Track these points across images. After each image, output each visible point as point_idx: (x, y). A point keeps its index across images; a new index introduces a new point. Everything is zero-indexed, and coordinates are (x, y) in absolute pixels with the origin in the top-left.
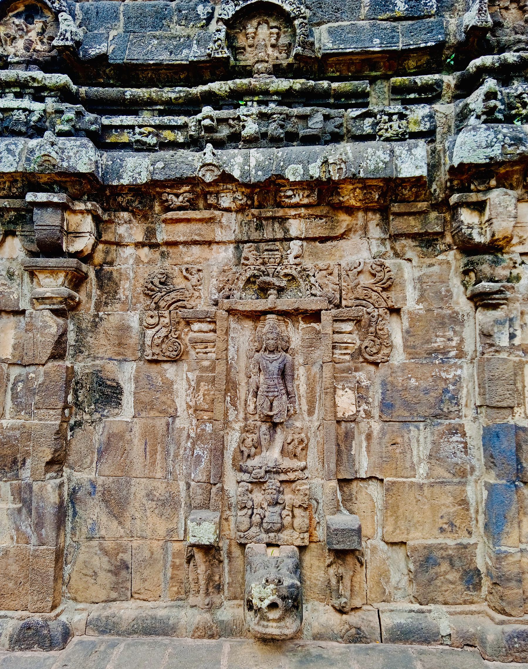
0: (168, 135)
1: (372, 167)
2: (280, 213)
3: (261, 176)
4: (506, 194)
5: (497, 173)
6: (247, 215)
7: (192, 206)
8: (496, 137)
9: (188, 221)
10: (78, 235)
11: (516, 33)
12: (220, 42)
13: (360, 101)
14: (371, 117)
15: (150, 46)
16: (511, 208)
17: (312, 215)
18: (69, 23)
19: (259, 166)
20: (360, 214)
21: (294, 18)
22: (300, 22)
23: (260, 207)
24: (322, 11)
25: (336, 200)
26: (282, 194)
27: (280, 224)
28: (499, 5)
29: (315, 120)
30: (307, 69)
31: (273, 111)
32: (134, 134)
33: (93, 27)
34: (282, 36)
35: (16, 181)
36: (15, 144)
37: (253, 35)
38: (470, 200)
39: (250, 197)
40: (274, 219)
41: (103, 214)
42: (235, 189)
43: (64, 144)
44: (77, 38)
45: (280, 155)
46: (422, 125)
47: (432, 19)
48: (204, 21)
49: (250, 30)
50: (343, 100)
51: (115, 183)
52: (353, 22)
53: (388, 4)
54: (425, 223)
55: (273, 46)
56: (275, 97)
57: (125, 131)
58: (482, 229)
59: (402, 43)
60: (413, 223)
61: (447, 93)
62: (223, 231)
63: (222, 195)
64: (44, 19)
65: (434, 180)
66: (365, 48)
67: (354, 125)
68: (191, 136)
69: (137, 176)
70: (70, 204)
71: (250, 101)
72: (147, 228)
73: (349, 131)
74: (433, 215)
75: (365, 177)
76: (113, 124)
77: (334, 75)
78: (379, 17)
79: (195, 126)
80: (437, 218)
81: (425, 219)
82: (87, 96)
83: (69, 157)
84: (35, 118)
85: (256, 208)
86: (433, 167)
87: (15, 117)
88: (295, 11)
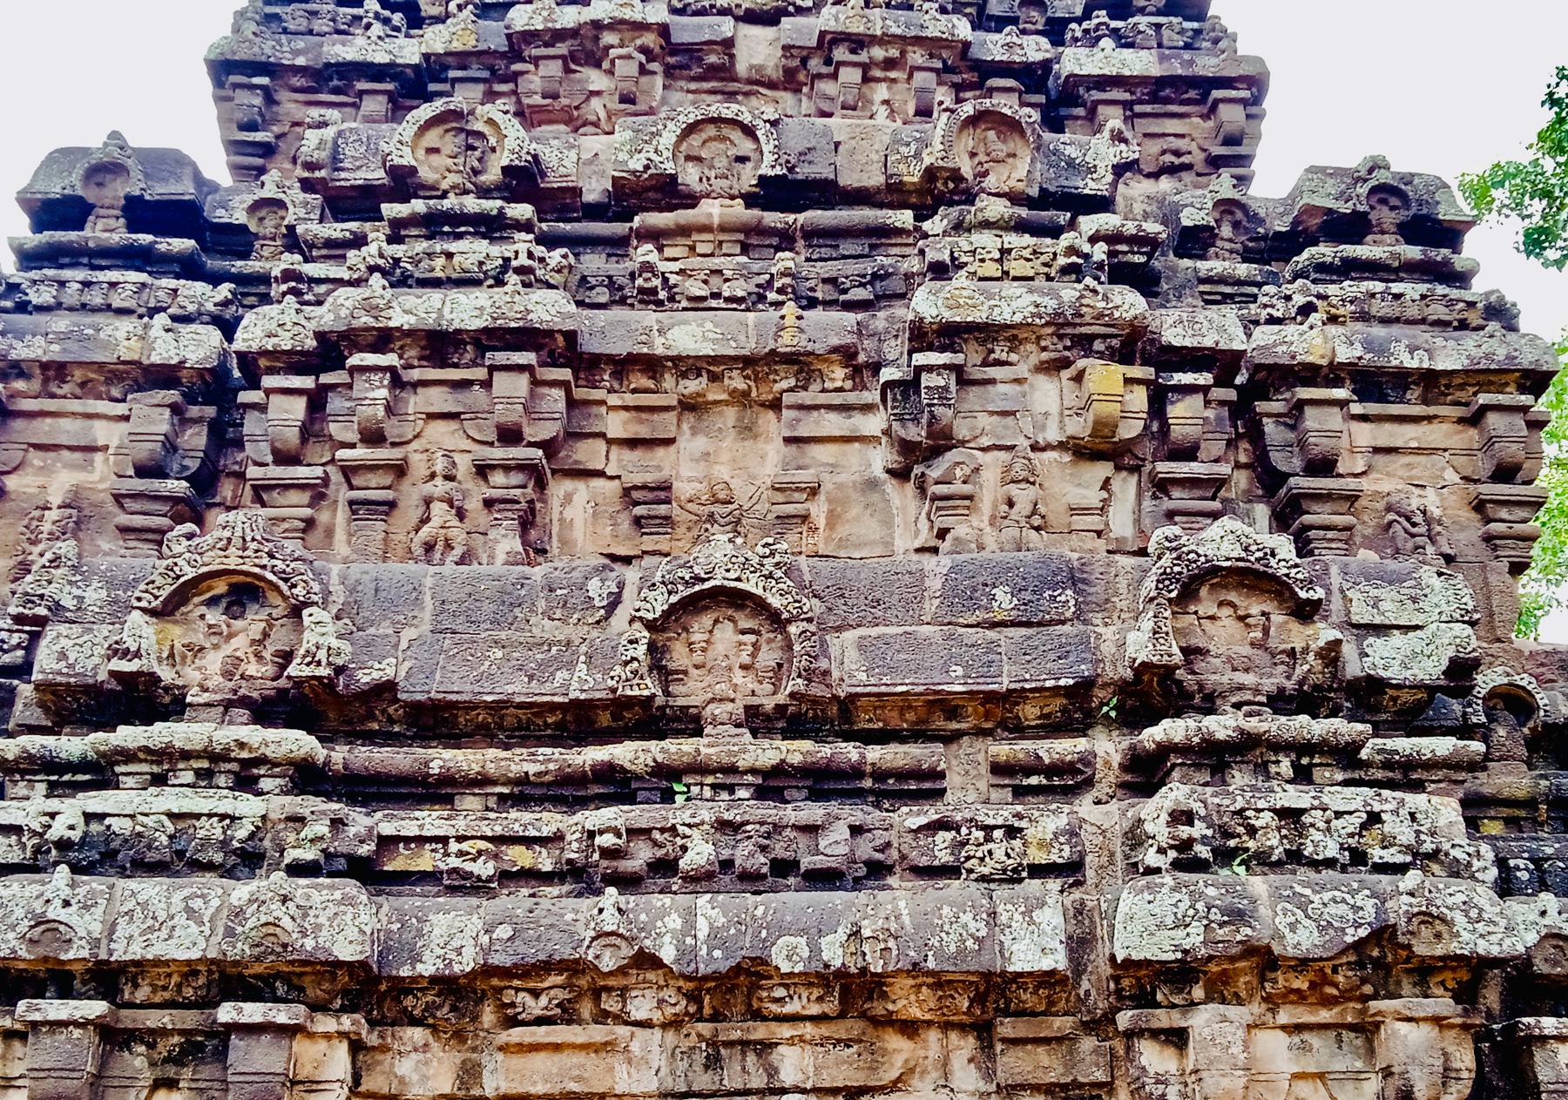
0: (520, 857)
1: (953, 948)
2: (760, 1031)
3: (719, 961)
4: (1224, 1019)
5: (1205, 973)
6: (687, 1035)
7: (568, 1015)
9: (557, 1047)
10: (315, 1087)
11: (1235, 669)
12: (635, 664)
13: (927, 785)
15: (487, 663)
16: (1236, 1049)
17: (828, 1038)
18: (324, 630)
20: (933, 1035)
21: (789, 621)
23: (716, 1017)
25: (878, 1008)
26: (765, 994)
27: (759, 1055)
28: (1196, 613)
29: (833, 837)
30: (815, 715)
31: (747, 817)
33: (366, 619)
34: (764, 648)
35: (196, 973)
36: (203, 896)
38: (1155, 1024)
39: (693, 997)
40: (744, 1044)
41: (370, 1032)
42: (662, 983)
43: (308, 897)
44: (340, 662)
45: (760, 912)
47: (1067, 628)
48: (602, 612)
49: (698, 638)
50: (891, 781)
51: (405, 972)
52: (908, 629)
54: (1071, 1063)
55: (744, 667)
56: (749, 778)
57: (427, 846)
58: (1186, 1085)
59: (1009, 676)
60: (1045, 1061)
61: (1107, 778)
62: (632, 1070)
63: (634, 993)
64: (268, 610)
68: (570, 862)
69: (453, 956)
70: (308, 1024)
72: (464, 1062)
73: (903, 857)
74: (1088, 1043)
76: (403, 833)
77: (871, 726)
79: (579, 840)
80: (1095, 1051)
81: (1070, 1053)
82: (345, 768)
83: (318, 927)
84: (242, 833)
85: (706, 1021)
86: (1079, 945)
87: (201, 833)
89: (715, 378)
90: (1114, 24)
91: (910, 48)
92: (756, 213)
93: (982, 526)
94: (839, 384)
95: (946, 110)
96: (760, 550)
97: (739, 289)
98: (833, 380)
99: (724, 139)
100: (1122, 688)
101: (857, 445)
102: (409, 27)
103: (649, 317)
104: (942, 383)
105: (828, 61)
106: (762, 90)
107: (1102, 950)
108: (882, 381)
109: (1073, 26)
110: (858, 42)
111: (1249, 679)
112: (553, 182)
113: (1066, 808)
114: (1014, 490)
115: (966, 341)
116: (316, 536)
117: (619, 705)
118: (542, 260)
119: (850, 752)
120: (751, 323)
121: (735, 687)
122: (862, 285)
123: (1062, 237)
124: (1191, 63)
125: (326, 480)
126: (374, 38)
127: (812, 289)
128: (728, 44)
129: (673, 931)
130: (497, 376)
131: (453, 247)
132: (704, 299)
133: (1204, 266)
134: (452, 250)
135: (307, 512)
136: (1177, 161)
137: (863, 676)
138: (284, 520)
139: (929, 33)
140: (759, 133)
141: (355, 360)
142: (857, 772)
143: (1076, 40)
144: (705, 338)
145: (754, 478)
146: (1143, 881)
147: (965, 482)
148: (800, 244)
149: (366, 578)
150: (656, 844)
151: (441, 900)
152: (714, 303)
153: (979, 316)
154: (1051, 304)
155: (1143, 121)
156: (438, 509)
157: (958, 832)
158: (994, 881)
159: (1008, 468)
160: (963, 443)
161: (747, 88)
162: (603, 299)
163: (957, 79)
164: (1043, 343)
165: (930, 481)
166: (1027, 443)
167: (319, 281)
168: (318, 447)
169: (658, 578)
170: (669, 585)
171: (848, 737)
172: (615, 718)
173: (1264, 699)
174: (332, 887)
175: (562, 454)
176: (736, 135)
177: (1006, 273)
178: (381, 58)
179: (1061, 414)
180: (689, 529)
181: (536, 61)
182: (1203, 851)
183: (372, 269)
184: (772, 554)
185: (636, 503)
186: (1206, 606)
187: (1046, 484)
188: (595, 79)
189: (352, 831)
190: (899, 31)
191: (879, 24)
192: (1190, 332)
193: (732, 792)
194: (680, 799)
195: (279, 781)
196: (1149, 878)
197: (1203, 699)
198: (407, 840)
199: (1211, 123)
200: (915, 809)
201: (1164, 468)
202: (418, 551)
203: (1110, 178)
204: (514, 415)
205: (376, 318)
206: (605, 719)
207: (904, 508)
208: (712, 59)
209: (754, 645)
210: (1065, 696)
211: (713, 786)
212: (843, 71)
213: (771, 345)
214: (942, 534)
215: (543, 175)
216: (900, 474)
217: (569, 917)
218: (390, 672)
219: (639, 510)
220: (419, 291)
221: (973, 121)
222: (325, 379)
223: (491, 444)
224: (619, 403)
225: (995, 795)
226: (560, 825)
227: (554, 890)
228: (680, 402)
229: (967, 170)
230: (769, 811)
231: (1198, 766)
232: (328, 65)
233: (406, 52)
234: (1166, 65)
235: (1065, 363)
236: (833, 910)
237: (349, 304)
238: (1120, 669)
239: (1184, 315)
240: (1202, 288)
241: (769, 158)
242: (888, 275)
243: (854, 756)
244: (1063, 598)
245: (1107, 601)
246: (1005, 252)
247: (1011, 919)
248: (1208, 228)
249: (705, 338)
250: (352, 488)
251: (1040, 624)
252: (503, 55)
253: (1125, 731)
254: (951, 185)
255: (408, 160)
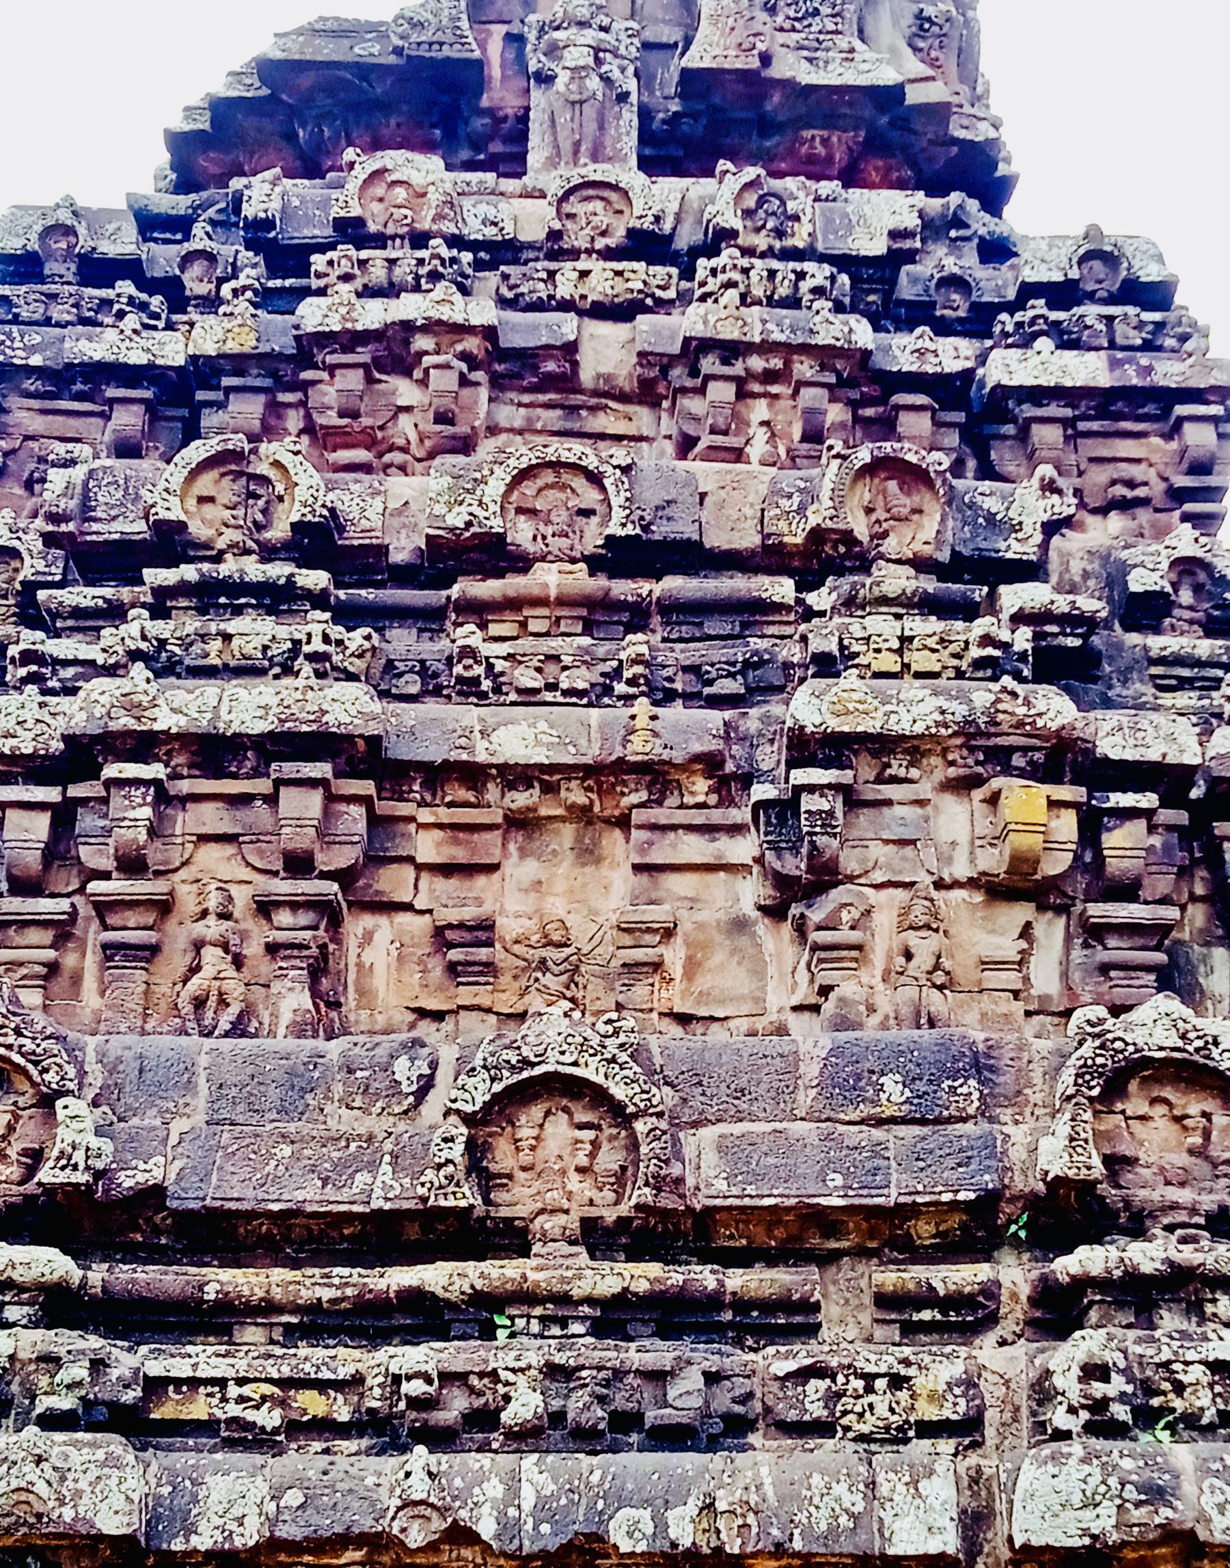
0: (312, 1404)
1: (823, 1526)
8: (1104, 1482)
11: (1168, 1183)
12: (451, 1168)
13: (798, 1319)
14: (822, 1377)
15: (273, 1163)
18: (81, 1126)
19: (543, 1508)
21: (635, 1116)
22: (650, 1126)
24: (703, 1094)
28: (1123, 1112)
30: (665, 1229)
31: (581, 1361)
32: (224, 1400)
34: (605, 1146)
37: (533, 1142)
43: (66, 1457)
44: (100, 1165)
45: (595, 1478)
46: (948, 1405)
47: (969, 1127)
49: (526, 1132)
50: (755, 1314)
51: (177, 1545)
52: (778, 1126)
53: (862, 1084)
56: (586, 1310)
57: (202, 1390)
61: (1013, 1315)
64: (13, 1098)
65: (980, 1552)
66: (810, 1196)
67: (781, 1395)
68: (371, 1411)
69: (233, 1526)
71: (521, 1316)
73: (768, 1410)
75: (806, 1550)
77: (732, 1243)
78: (842, 1116)
88: (636, 1100)
89: (550, 789)
90: (1055, 316)
91: (795, 357)
92: (602, 582)
93: (873, 982)
94: (701, 798)
95: (835, 457)
96: (601, 1027)
97: (580, 679)
98: (692, 793)
99: (564, 487)
100: (1031, 1201)
101: (722, 874)
102: (172, 310)
103: (469, 715)
104: (827, 807)
105: (694, 372)
106: (611, 404)
107: (1001, 1527)
108: (753, 799)
109: (1004, 316)
110: (731, 350)
111: (1184, 1196)
112: (353, 538)
113: (963, 1351)
114: (912, 938)
115: (856, 753)
116: (60, 984)
117: (429, 1216)
118: (340, 643)
119: (706, 1277)
120: (594, 724)
121: (570, 1196)
122: (732, 675)
123: (978, 621)
124: (1149, 370)
125: (73, 914)
126: (128, 332)
127: (670, 680)
128: (570, 349)
129: (494, 1500)
130: (283, 791)
131: (232, 626)
132: (537, 691)
133: (1157, 643)
134: (231, 631)
135: (50, 954)
136: (1129, 494)
137: (721, 1185)
138: (21, 964)
139: (819, 340)
140: (607, 482)
141: (111, 771)
142: (715, 1300)
143: (1006, 335)
144: (538, 742)
145: (597, 913)
146: (1047, 1450)
147: (853, 928)
148: (656, 620)
149: (128, 1055)
150: (472, 1391)
151: (219, 1456)
152: (548, 696)
153: (871, 725)
154: (961, 710)
155: (1089, 442)
156: (211, 955)
157: (834, 1381)
158: (875, 1441)
159: (905, 911)
160: (851, 879)
161: (593, 401)
162: (414, 689)
163: (855, 395)
164: (950, 757)
165: (811, 925)
166: (929, 880)
167: (66, 663)
168: (63, 874)
169: (478, 1062)
170: (493, 1070)
171: (706, 1258)
172: (425, 1230)
173: (1202, 1221)
174: (94, 1445)
175: (361, 883)
176: (579, 483)
177: (906, 666)
178: (137, 358)
179: (973, 843)
180: (515, 977)
181: (332, 369)
182: (1121, 1412)
183: (135, 655)
184: (616, 1033)
185: (451, 945)
186: (1136, 1104)
187: (952, 931)
188: (404, 391)
189: (114, 1374)
190: (781, 338)
191: (758, 327)
192: (1132, 742)
193: (564, 1326)
194: (502, 1334)
195: (26, 1309)
196: (1054, 1445)
197: (1129, 1219)
198: (178, 1382)
199: (1174, 445)
200: (783, 1349)
201: (1098, 911)
202: (187, 1009)
203: (1038, 538)
204: (304, 839)
205: (138, 719)
206: (413, 1232)
207: (779, 955)
208: (550, 366)
209: (592, 1143)
210: (965, 1211)
211: (542, 1319)
212: (712, 386)
213: (618, 752)
214: (825, 991)
215: (341, 529)
216: (774, 912)
217: (370, 1481)
218: (158, 1174)
219: (454, 955)
220: (190, 683)
221: (869, 470)
222: (75, 791)
223: (275, 874)
224: (432, 820)
225: (879, 1332)
226: (359, 1366)
227: (351, 1445)
228: (505, 816)
229: (861, 530)
230: (610, 1353)
231: (1120, 1305)
232: (69, 366)
233: (167, 350)
234: (1117, 373)
235: (979, 782)
236: (683, 1478)
237: (104, 699)
238: (1031, 1180)
239: (1125, 720)
240: (1154, 670)
241: (618, 514)
242: (762, 663)
243: (711, 1284)
244: (964, 1090)
245: (1019, 1093)
246: (905, 640)
247: (893, 1491)
248: (1161, 595)
249: (538, 742)
250: (106, 927)
251: (938, 1121)
252: (288, 359)
253: (1038, 1253)
254: (842, 549)
255: (176, 514)
